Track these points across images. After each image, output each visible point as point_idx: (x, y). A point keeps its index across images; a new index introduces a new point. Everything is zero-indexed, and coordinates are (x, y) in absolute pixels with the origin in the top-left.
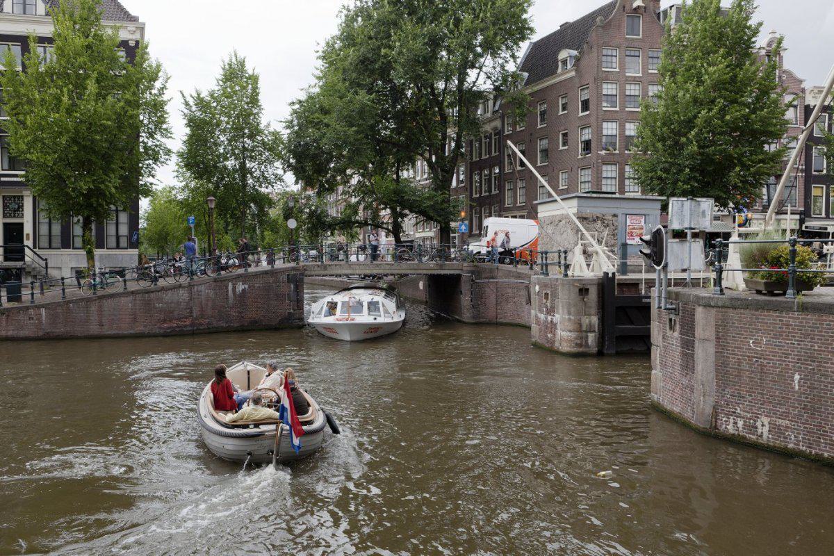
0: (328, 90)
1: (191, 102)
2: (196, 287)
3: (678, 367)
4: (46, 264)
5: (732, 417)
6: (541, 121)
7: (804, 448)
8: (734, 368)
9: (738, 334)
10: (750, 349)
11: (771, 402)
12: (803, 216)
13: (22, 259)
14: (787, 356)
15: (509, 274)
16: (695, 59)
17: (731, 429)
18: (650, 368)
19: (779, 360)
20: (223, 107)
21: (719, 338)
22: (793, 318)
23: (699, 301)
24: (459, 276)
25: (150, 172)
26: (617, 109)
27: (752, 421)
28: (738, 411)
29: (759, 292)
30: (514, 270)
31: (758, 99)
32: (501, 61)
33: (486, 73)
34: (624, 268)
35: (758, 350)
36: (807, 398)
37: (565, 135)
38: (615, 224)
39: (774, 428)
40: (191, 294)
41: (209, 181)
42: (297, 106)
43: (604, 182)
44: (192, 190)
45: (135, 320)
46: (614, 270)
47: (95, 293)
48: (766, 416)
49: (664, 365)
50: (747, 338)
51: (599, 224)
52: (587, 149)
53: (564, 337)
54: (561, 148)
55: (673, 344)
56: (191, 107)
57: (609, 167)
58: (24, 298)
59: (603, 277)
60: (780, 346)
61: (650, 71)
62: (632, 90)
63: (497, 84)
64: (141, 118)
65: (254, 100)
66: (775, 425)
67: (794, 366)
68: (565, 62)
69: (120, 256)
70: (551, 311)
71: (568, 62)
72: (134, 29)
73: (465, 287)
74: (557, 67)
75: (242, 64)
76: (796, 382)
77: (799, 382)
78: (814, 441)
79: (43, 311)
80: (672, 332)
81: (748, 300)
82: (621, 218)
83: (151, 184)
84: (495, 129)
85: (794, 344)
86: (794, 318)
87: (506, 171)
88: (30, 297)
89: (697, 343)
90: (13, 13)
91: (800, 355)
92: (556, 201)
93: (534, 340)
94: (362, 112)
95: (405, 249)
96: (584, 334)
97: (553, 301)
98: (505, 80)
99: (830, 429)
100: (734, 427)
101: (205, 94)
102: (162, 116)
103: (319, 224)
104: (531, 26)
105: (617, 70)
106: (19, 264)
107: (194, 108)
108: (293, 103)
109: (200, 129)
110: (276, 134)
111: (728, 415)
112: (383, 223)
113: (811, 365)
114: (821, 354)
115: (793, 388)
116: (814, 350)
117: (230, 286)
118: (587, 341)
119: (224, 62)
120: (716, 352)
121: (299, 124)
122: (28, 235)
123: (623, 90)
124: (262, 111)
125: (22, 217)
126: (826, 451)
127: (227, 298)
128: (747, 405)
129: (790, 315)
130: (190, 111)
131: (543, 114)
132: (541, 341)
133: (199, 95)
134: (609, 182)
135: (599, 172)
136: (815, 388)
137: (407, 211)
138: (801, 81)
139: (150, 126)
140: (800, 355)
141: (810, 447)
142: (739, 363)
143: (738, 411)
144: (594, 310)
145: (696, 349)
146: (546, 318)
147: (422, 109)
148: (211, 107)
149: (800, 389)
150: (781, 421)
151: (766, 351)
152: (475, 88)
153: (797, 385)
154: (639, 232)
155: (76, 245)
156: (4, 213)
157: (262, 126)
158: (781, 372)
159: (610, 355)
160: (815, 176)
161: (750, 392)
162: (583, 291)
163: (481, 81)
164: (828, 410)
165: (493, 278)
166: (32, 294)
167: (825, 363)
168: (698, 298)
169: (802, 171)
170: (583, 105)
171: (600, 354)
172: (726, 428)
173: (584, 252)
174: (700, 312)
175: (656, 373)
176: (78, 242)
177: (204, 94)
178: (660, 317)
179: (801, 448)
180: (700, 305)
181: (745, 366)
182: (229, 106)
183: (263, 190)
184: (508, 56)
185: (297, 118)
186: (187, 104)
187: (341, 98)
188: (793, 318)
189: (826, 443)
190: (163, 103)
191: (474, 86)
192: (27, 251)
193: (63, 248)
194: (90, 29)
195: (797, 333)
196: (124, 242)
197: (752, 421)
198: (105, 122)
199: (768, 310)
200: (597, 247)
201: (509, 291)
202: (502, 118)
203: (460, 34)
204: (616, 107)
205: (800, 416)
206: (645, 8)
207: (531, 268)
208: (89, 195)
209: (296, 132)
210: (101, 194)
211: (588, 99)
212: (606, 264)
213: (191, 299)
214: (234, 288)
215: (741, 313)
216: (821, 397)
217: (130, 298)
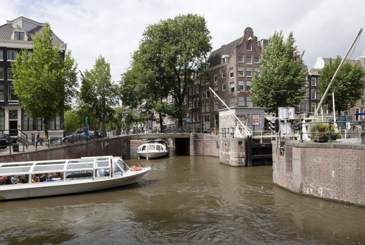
0: (136, 69)
1: (84, 74)
3: (285, 170)
4: (27, 136)
7: (337, 199)
11: (323, 182)
14: (329, 164)
17: (308, 193)
19: (326, 166)
22: (331, 150)
26: (244, 76)
27: (316, 189)
28: (311, 185)
29: (316, 141)
33: (195, 63)
34: (254, 134)
35: (318, 163)
39: (325, 192)
49: (278, 169)
52: (233, 91)
53: (233, 160)
55: (282, 161)
58: (20, 150)
59: (247, 138)
62: (248, 69)
63: (199, 67)
65: (108, 74)
66: (325, 190)
68: (224, 59)
70: (228, 150)
71: (225, 59)
75: (103, 60)
76: (333, 174)
77: (334, 174)
79: (28, 155)
81: (313, 144)
83: (71, 105)
86: (332, 151)
88: (23, 149)
89: (293, 161)
90: (15, 39)
92: (228, 109)
93: (220, 161)
94: (150, 78)
97: (228, 146)
100: (309, 191)
101: (89, 71)
103: (131, 120)
104: (212, 46)
105: (243, 62)
106: (16, 137)
107: (85, 76)
108: (122, 75)
109: (86, 86)
110: (116, 86)
111: (307, 187)
112: (156, 119)
113: (339, 168)
116: (340, 162)
117: (102, 144)
118: (242, 161)
120: (301, 164)
122: (19, 125)
123: (245, 70)
125: (17, 118)
126: (345, 199)
127: (101, 149)
128: (314, 183)
134: (249, 103)
137: (167, 115)
138: (307, 67)
142: (310, 167)
143: (311, 185)
144: (244, 150)
146: (226, 153)
150: (327, 189)
152: (191, 69)
153: (333, 175)
154: (257, 120)
155: (39, 129)
156: (10, 117)
157: (111, 83)
161: (315, 178)
163: (193, 66)
164: (346, 184)
165: (202, 139)
166: (24, 148)
167: (344, 167)
168: (293, 144)
169: (308, 98)
171: (246, 166)
172: (306, 192)
173: (240, 129)
174: (294, 149)
178: (276, 151)
179: (335, 198)
180: (294, 147)
181: (313, 169)
183: (112, 107)
184: (203, 57)
186: (82, 75)
187: (142, 72)
189: (345, 196)
195: (333, 156)
196: (58, 128)
197: (316, 189)
198: (53, 80)
202: (201, 79)
204: (243, 75)
205: (335, 186)
206: (253, 40)
207: (216, 135)
209: (124, 85)
210: (51, 109)
212: (247, 133)
214: (104, 145)
215: (311, 149)
216: (343, 179)
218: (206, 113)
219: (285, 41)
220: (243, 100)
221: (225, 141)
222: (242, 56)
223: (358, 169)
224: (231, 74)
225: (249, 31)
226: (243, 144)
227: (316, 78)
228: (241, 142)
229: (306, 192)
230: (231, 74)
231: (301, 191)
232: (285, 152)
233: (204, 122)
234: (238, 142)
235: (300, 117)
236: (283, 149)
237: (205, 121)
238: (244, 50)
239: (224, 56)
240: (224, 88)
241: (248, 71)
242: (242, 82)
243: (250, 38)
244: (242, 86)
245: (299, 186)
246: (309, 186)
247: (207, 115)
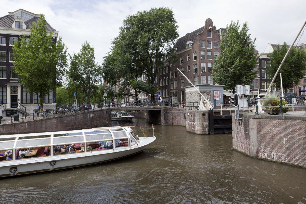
0: (116, 53)
1: (72, 57)
3: (243, 138)
4: (25, 108)
5: (263, 153)
6: (182, 63)
7: (288, 162)
9: (264, 127)
13: (17, 107)
14: (281, 133)
15: (176, 110)
17: (263, 157)
18: (232, 138)
20: (83, 58)
22: (283, 121)
23: (250, 117)
24: (160, 111)
25: (61, 78)
26: (205, 59)
27: (270, 154)
30: (178, 108)
31: (249, 56)
33: (165, 48)
34: (215, 107)
39: (278, 156)
40: (76, 118)
41: (78, 81)
42: (105, 58)
43: (202, 81)
44: (71, 85)
45: (57, 126)
47: (44, 118)
48: (275, 152)
49: (237, 137)
50: (267, 128)
51: (205, 94)
53: (198, 128)
54: (188, 71)
55: (241, 130)
56: (72, 58)
57: (203, 77)
58: (20, 120)
60: (279, 130)
61: (214, 48)
62: (209, 53)
63: (168, 51)
64: (58, 61)
65: (92, 56)
66: (278, 155)
67: (283, 136)
68: (188, 45)
69: (50, 106)
70: (193, 121)
73: (162, 114)
74: (186, 47)
75: (88, 45)
76: (284, 141)
77: (285, 141)
78: (291, 159)
80: (240, 126)
82: (212, 92)
84: (167, 65)
85: (283, 129)
86: (283, 122)
87: (171, 78)
89: (250, 130)
90: (15, 28)
91: (285, 133)
92: (193, 86)
93: (187, 130)
95: (138, 102)
96: (204, 128)
97: (194, 118)
102: (65, 60)
105: (205, 47)
106: (16, 109)
107: (73, 59)
108: (104, 57)
110: (99, 66)
111: (262, 152)
112: (132, 94)
113: (289, 136)
114: (292, 132)
115: (284, 143)
117: (88, 115)
119: (82, 44)
121: (106, 64)
122: (19, 99)
123: (206, 54)
124: (95, 59)
126: (295, 163)
129: (282, 120)
130: (72, 59)
131: (182, 61)
133: (75, 54)
135: (200, 78)
136: (291, 143)
138: (258, 51)
139: (62, 64)
140: (285, 133)
141: (289, 162)
142: (265, 136)
143: (265, 151)
144: (207, 121)
145: (250, 132)
146: (192, 123)
147: (146, 59)
148: (79, 58)
149: (286, 144)
152: (162, 53)
154: (217, 96)
155: (35, 102)
157: (95, 64)
158: (279, 138)
159: (227, 133)
160: (263, 79)
161: (269, 145)
162: (204, 115)
163: (163, 50)
166: (23, 118)
167: (294, 135)
170: (194, 58)
171: (209, 134)
172: (261, 156)
173: (203, 103)
174: (251, 121)
175: (235, 140)
176: (36, 101)
179: (287, 162)
180: (251, 118)
181: (267, 137)
182: (84, 58)
183: (95, 84)
184: (171, 43)
186: (71, 57)
187: (120, 55)
188: (283, 121)
191: (161, 52)
192: (19, 104)
193: (31, 103)
194: (42, 33)
195: (284, 126)
196: (51, 101)
197: (270, 154)
199: (274, 119)
200: (207, 101)
201: (176, 115)
202: (169, 62)
205: (286, 152)
206: (212, 29)
208: (40, 85)
209: (106, 66)
211: (196, 56)
212: (210, 106)
213: (76, 119)
214: (89, 116)
215: (265, 120)
217: (56, 119)
220: (204, 79)
222: (204, 43)
225: (209, 22)
226: (207, 116)
227: (265, 61)
228: (205, 114)
229: (261, 156)
231: (257, 155)
232: (243, 123)
234: (202, 114)
235: (253, 94)
236: (241, 120)
237: (173, 97)
241: (209, 55)
243: (210, 28)
246: (264, 151)
247: (175, 91)
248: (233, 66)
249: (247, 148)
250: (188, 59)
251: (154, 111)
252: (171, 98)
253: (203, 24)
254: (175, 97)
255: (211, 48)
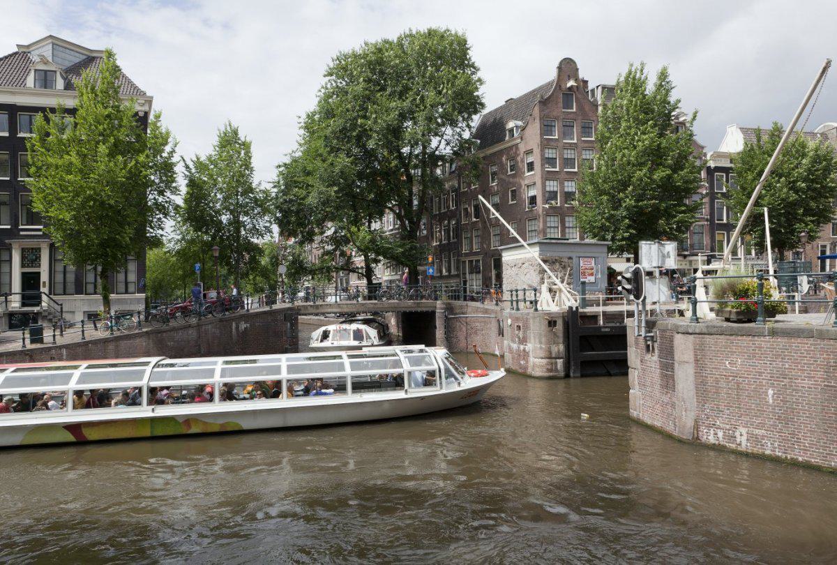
1: (191, 165)
2: (204, 327)
3: (657, 387)
4: (62, 308)
5: (712, 429)
7: (780, 454)
8: (713, 386)
10: (726, 369)
12: (709, 257)
13: (39, 304)
14: (760, 374)
15: (477, 310)
16: (630, 128)
17: (712, 440)
19: (753, 378)
21: (698, 361)
26: (557, 169)
28: (718, 423)
29: (728, 320)
32: (458, 130)
34: (585, 303)
36: (780, 410)
37: (514, 192)
38: (571, 265)
39: (752, 438)
42: (281, 169)
46: (577, 304)
47: (112, 334)
49: (642, 385)
54: (510, 202)
60: (753, 366)
61: (583, 139)
62: (569, 154)
63: (455, 149)
65: (247, 165)
68: (511, 131)
70: (523, 341)
72: (144, 102)
74: (505, 135)
75: (235, 132)
76: (770, 396)
77: (773, 397)
78: (788, 447)
83: (162, 236)
86: (765, 342)
89: (676, 365)
90: (35, 87)
92: (523, 246)
98: (461, 147)
99: (802, 436)
103: (299, 269)
105: (556, 137)
106: (36, 309)
107: (193, 171)
108: (280, 166)
110: (265, 192)
111: (709, 427)
112: (357, 268)
113: (783, 381)
114: (791, 372)
115: (768, 402)
117: (234, 325)
122: (44, 283)
123: (561, 155)
125: (39, 266)
126: (800, 456)
132: (514, 367)
133: (198, 159)
136: (787, 401)
137: (381, 258)
138: (703, 148)
142: (717, 381)
143: (718, 423)
144: (561, 340)
150: (757, 431)
151: (741, 371)
152: (437, 153)
153: (771, 399)
154: (590, 272)
155: (88, 291)
156: (22, 263)
157: (254, 185)
159: (616, 375)
161: (729, 407)
165: (463, 313)
166: (54, 336)
167: (796, 379)
171: (567, 376)
172: (707, 438)
173: (550, 290)
174: (678, 339)
175: (634, 392)
177: (203, 158)
178: (637, 343)
179: (777, 453)
180: (678, 333)
181: (723, 384)
183: (255, 240)
184: (464, 125)
185: (284, 179)
186: (187, 167)
187: (324, 161)
188: (763, 341)
190: (173, 165)
191: (436, 150)
196: (132, 288)
197: (731, 432)
201: (478, 324)
203: (425, 107)
205: (774, 426)
206: (577, 87)
207: (497, 304)
209: (283, 191)
212: (568, 300)
214: (237, 327)
215: (717, 339)
218: (472, 253)
219: (650, 88)
221: (517, 319)
222: (553, 124)
223: (827, 386)
224: (528, 164)
225: (567, 67)
226: (560, 326)
227: (725, 175)
228: (555, 322)
229: (707, 438)
230: (528, 164)
231: (696, 435)
232: (656, 345)
233: (467, 274)
235: (691, 264)
238: (558, 110)
239: (511, 125)
240: (514, 197)
242: (555, 182)
244: (554, 192)
245: (690, 423)
247: (474, 258)
248: (630, 188)
249: (669, 415)
250: (511, 170)
251: (416, 313)
252: (465, 278)
253: (551, 75)
254: (474, 274)
255: (573, 139)
